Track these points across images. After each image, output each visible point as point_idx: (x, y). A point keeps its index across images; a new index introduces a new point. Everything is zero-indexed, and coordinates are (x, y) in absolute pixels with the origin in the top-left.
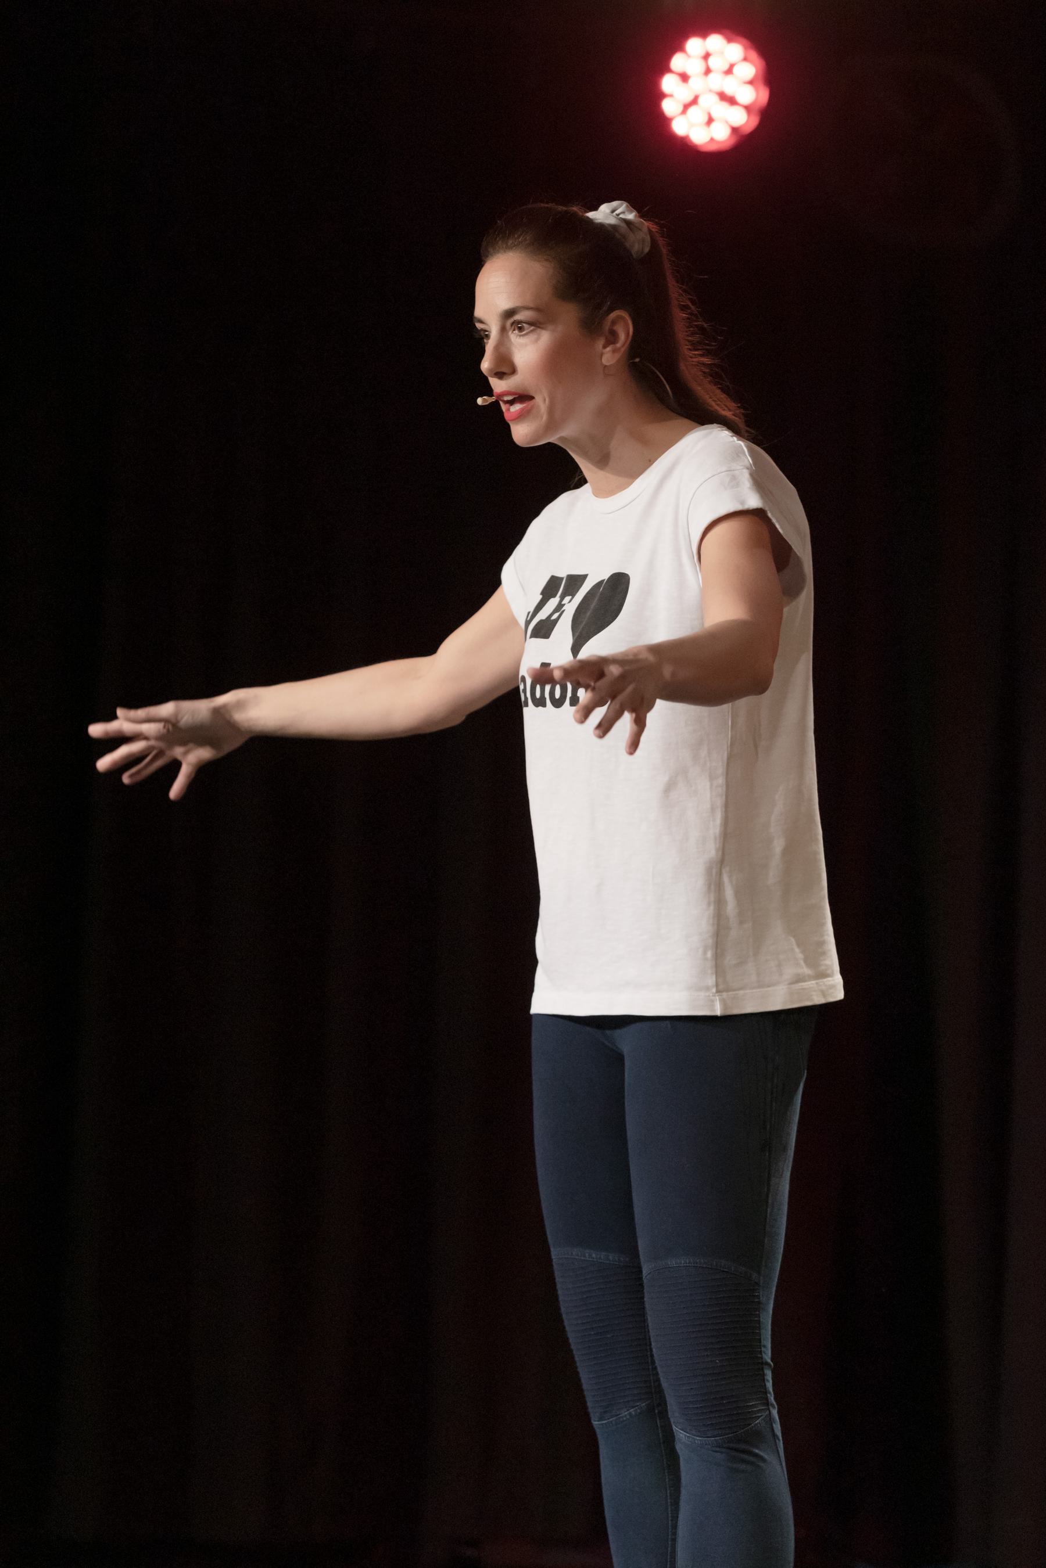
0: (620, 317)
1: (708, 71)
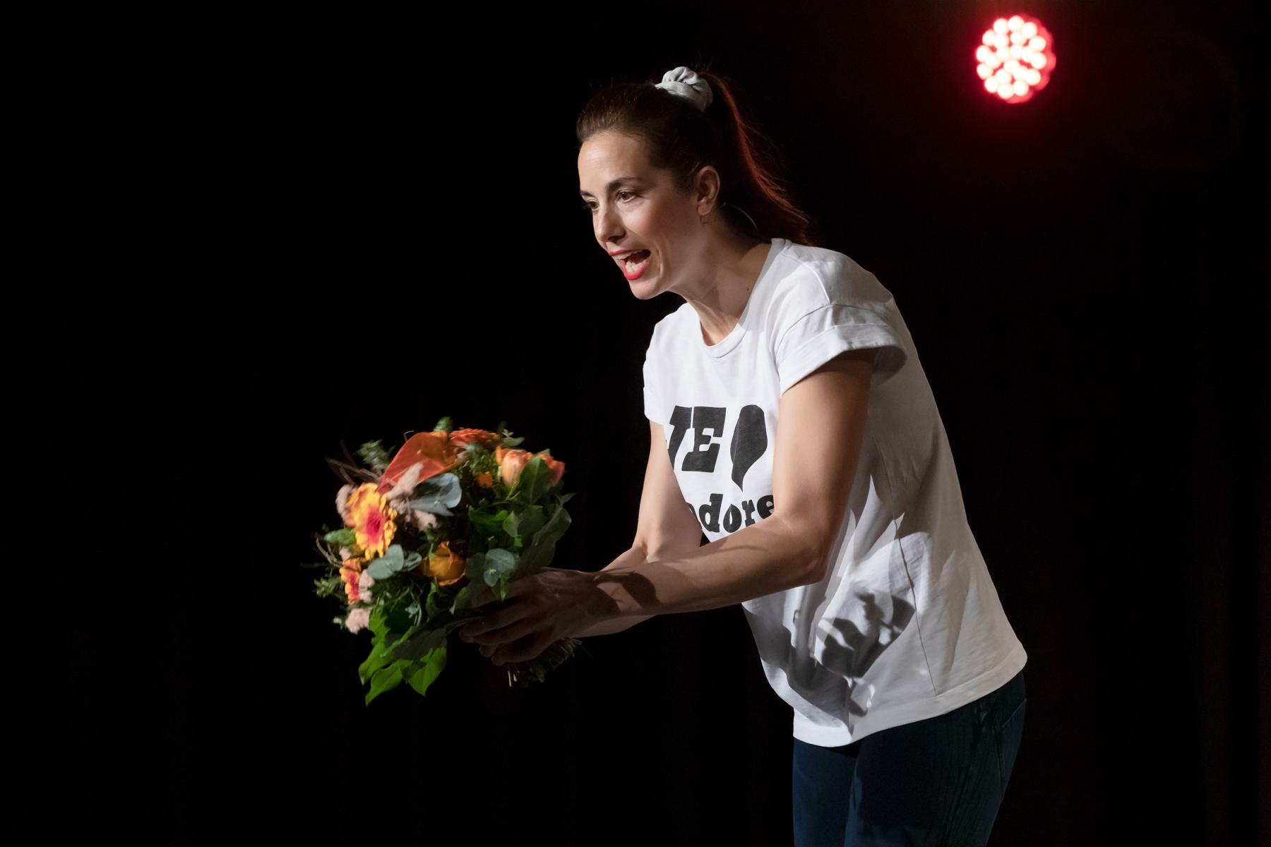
0: (707, 172)
1: (1010, 44)
